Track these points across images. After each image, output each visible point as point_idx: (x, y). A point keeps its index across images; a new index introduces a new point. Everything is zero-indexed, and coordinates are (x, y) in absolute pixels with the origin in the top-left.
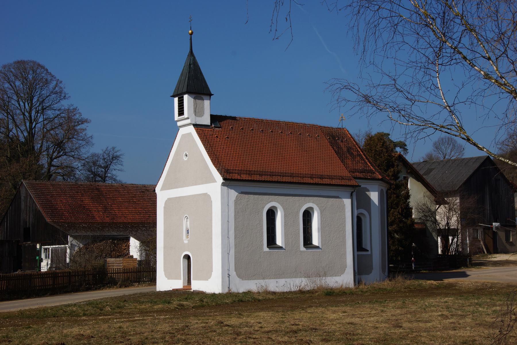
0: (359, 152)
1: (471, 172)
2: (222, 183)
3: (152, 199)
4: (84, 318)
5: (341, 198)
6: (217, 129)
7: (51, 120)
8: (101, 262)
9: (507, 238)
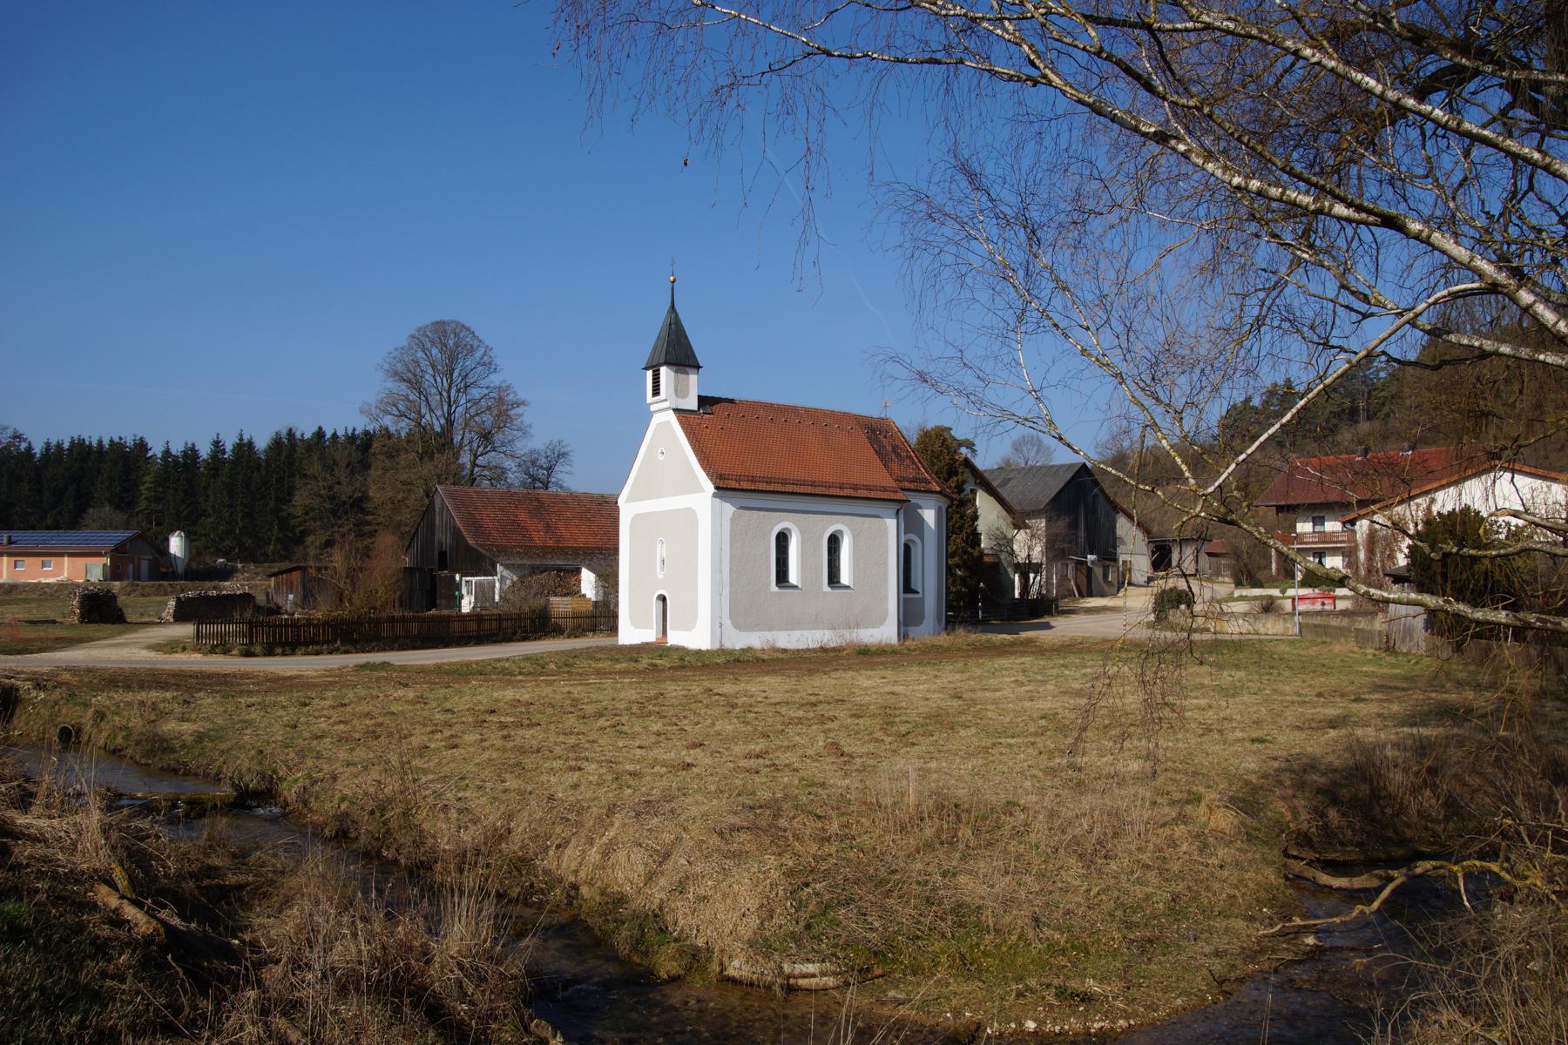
1: (1062, 484)
4: (520, 677)
7: (476, 402)
8: (542, 601)
9: (1105, 576)
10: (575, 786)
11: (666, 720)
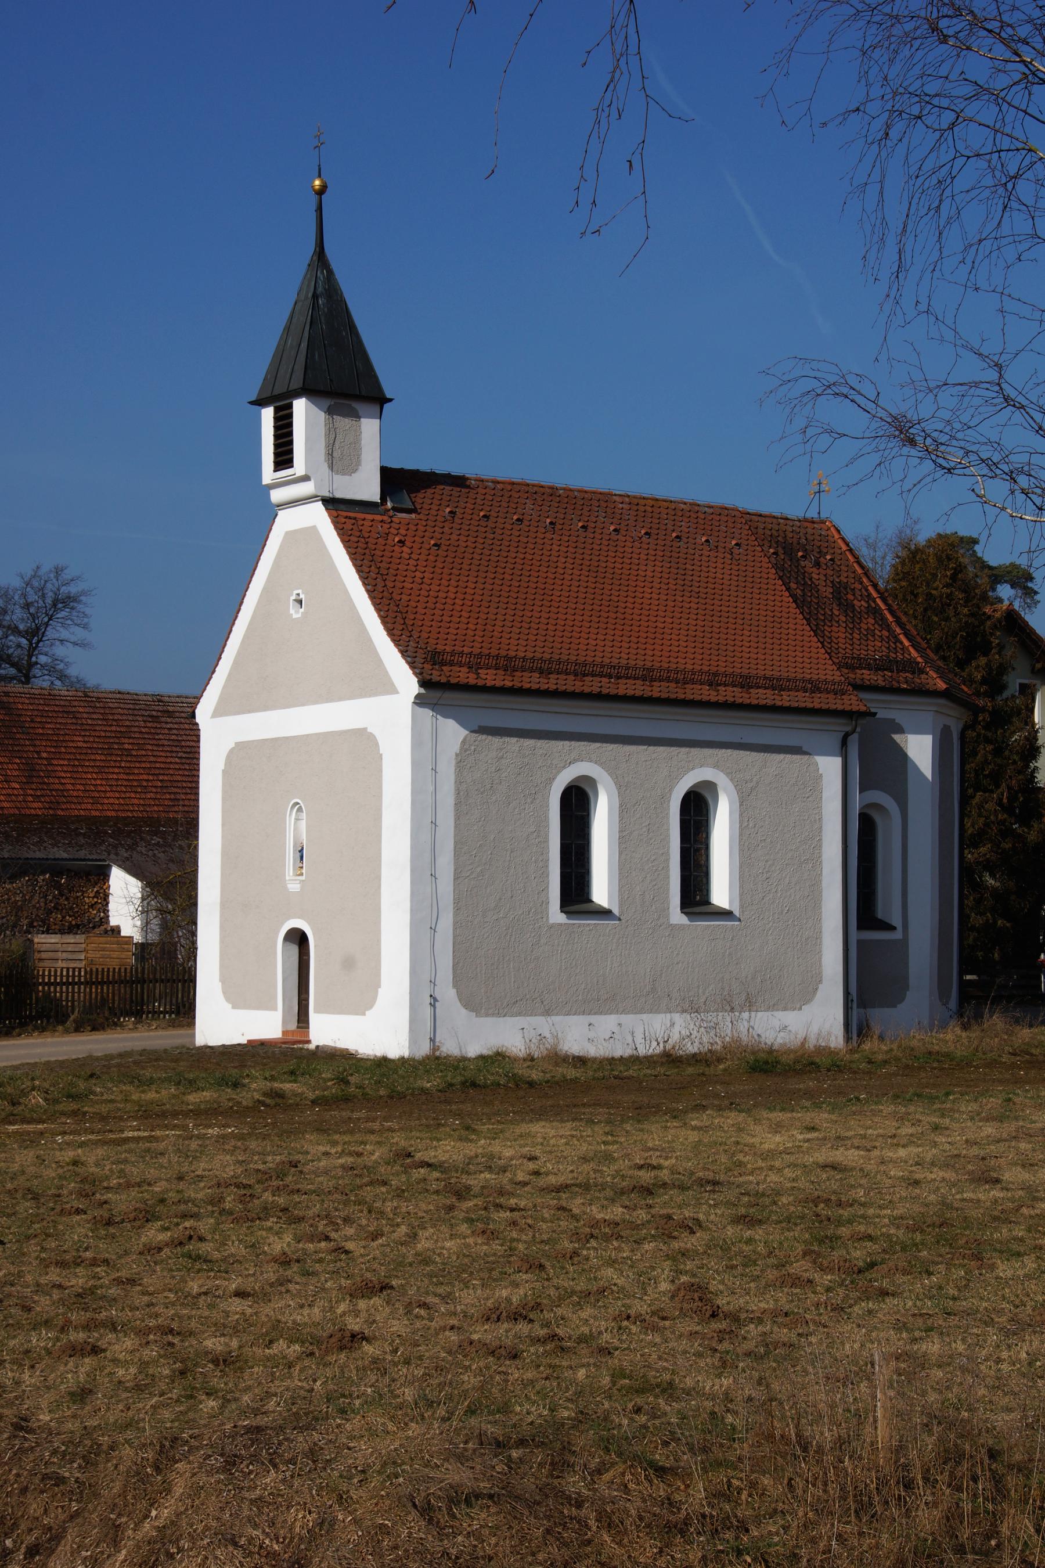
0: (875, 602)
3: (183, 743)
6: (404, 515)
10: (82, 1395)
11: (305, 1227)
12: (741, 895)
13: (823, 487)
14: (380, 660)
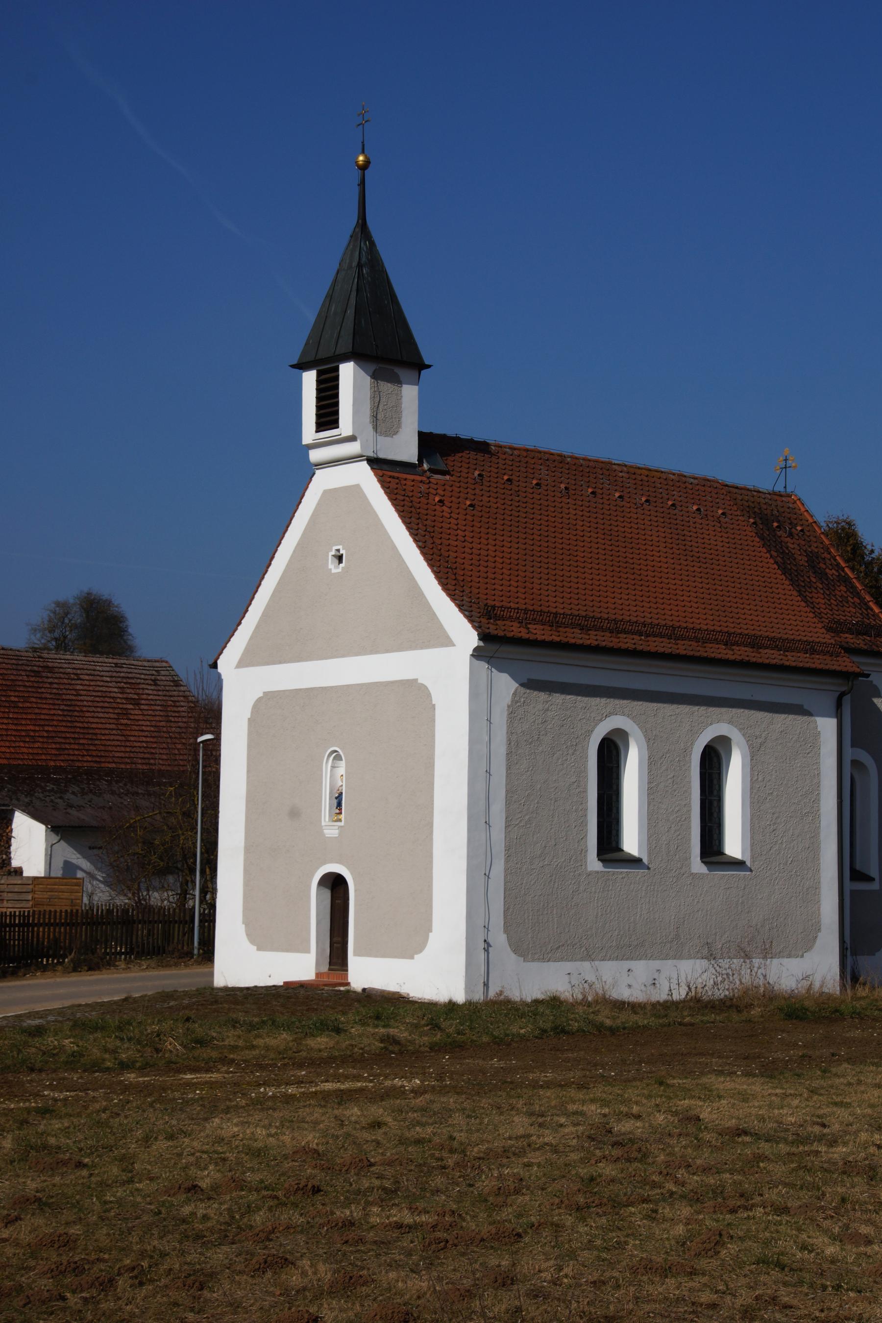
0: (843, 571)
2: (475, 650)
3: (64, 697)
5: (809, 714)
12: (752, 845)
13: (789, 463)
14: (434, 614)
